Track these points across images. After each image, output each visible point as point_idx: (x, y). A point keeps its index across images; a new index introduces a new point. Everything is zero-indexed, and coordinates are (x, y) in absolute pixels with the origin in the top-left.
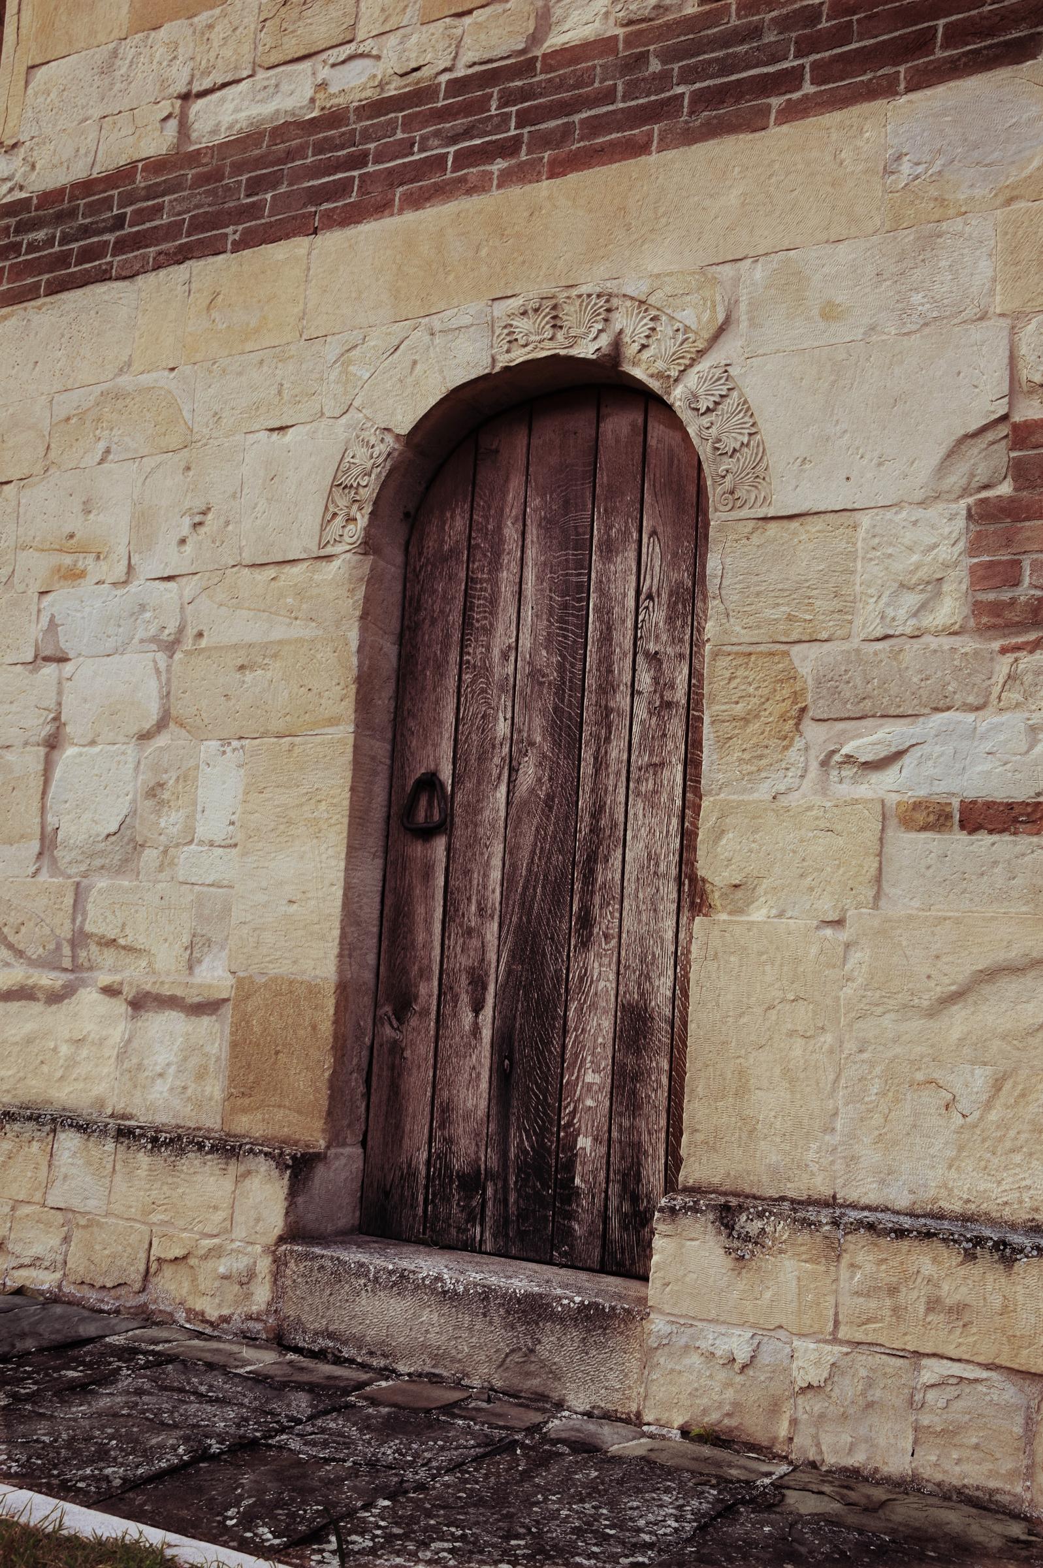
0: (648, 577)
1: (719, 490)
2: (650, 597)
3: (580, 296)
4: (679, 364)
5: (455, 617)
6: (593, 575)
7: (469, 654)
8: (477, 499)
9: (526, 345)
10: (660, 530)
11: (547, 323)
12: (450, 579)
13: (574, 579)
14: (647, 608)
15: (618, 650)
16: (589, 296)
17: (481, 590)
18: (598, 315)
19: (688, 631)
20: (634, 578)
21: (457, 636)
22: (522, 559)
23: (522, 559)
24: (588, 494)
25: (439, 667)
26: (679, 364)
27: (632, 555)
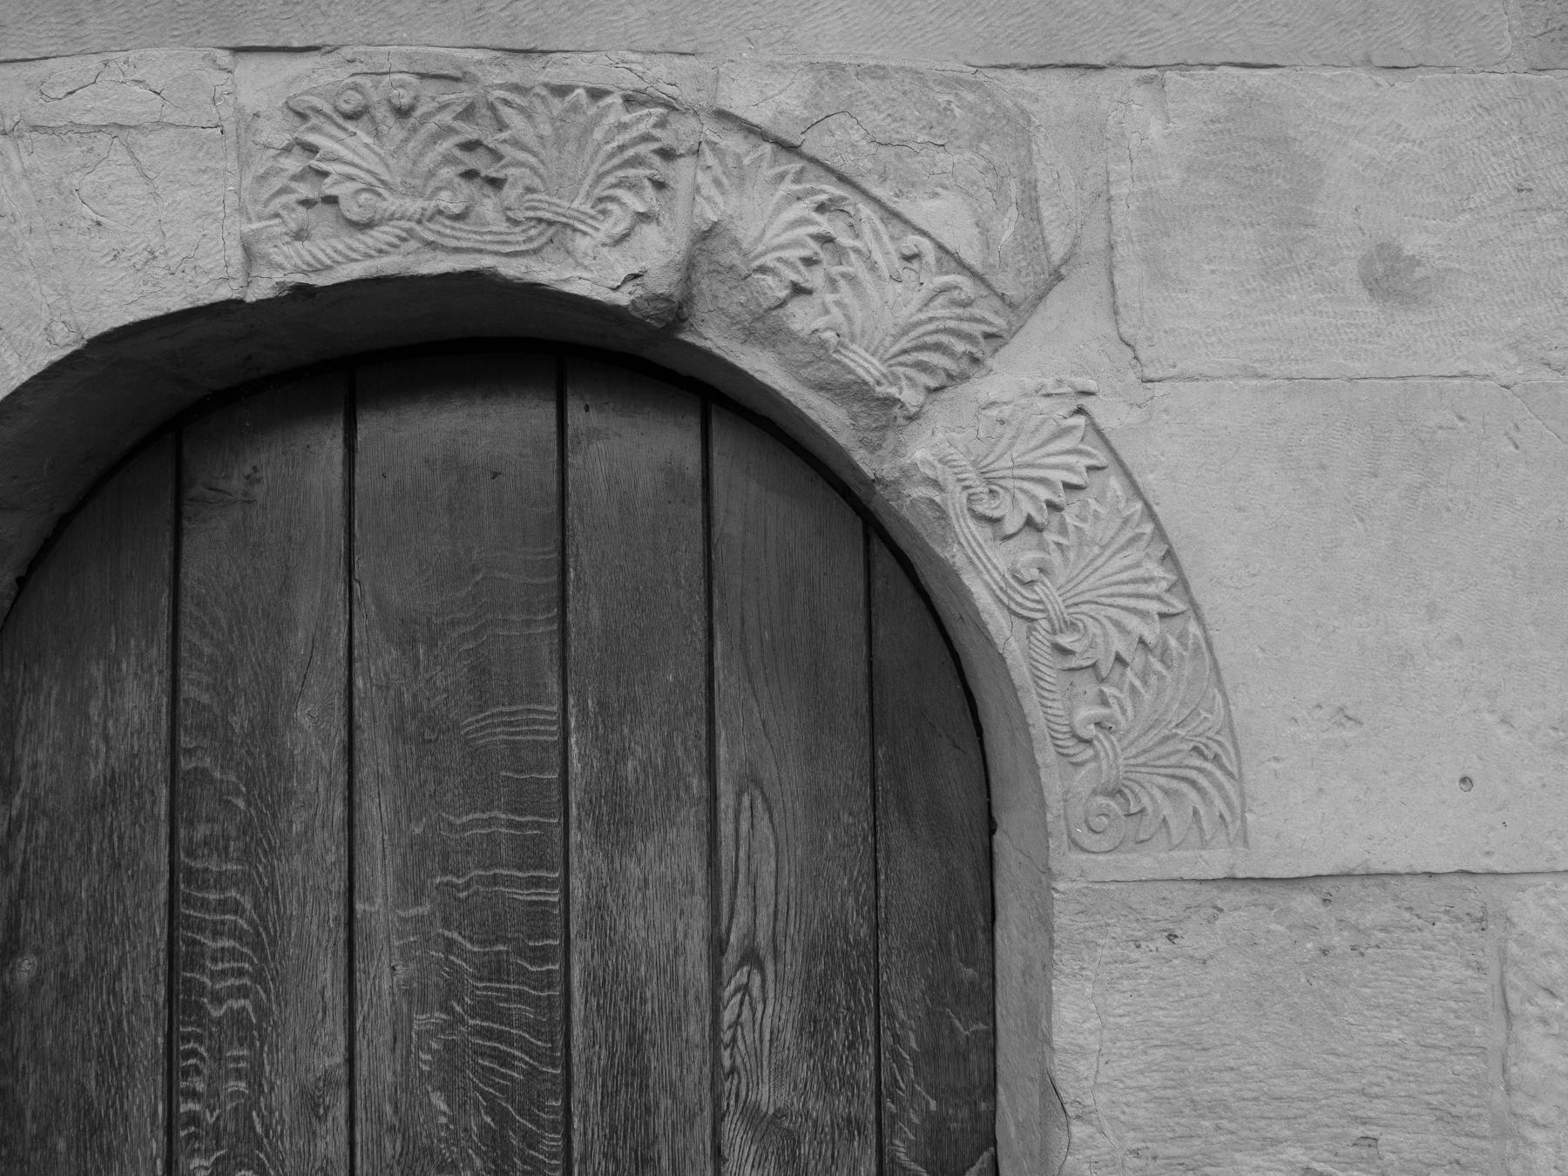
0: (741, 902)
1: (1082, 781)
2: (751, 957)
3: (562, 91)
4: (922, 367)
5: (143, 985)
6: (577, 884)
7: (193, 1095)
8: (188, 634)
9: (367, 226)
10: (768, 772)
11: (448, 160)
12: (117, 866)
13: (525, 895)
14: (745, 989)
15: (665, 1102)
16: (596, 94)
17: (223, 906)
18: (636, 162)
19: (868, 1059)
20: (700, 903)
21: (151, 1040)
22: (350, 824)
23: (350, 824)
24: (546, 652)
25: (96, 1130)
26: (922, 367)
27: (686, 833)
